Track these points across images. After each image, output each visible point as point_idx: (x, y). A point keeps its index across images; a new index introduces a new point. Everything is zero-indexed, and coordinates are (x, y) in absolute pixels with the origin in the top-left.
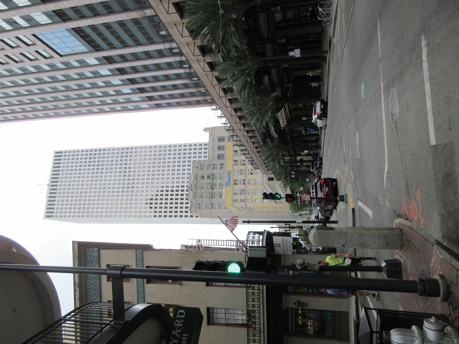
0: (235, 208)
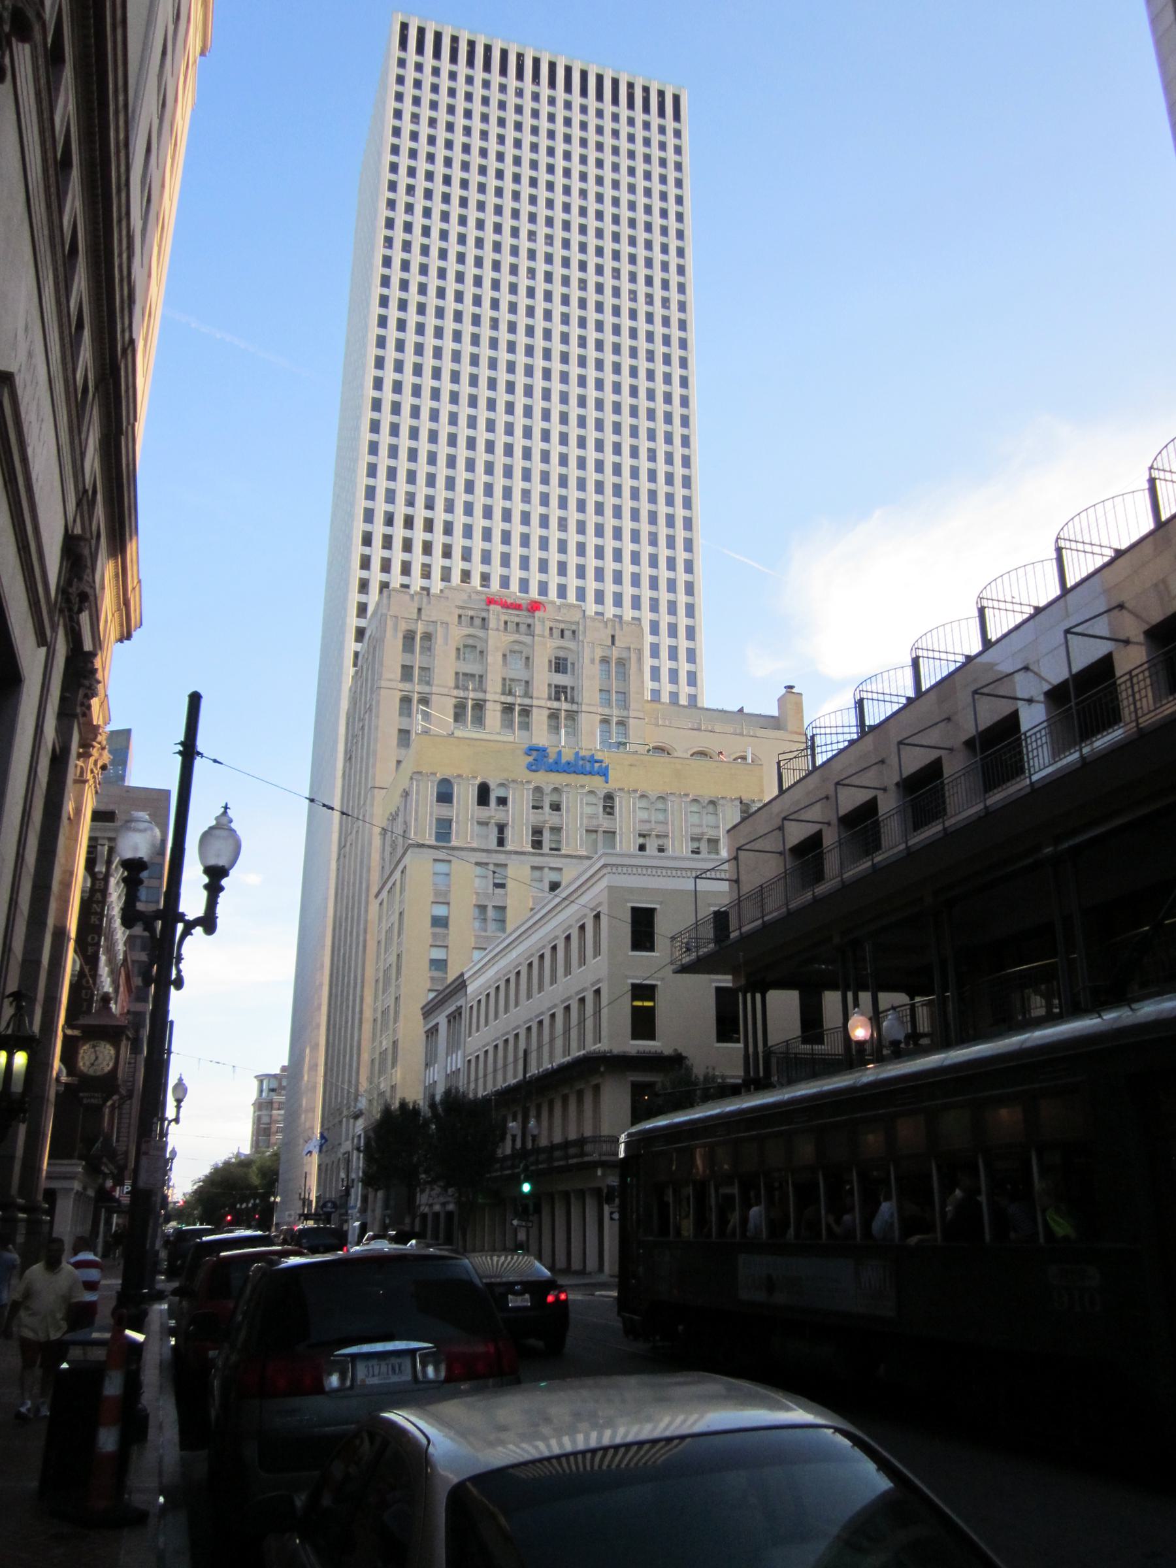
0: (406, 794)
